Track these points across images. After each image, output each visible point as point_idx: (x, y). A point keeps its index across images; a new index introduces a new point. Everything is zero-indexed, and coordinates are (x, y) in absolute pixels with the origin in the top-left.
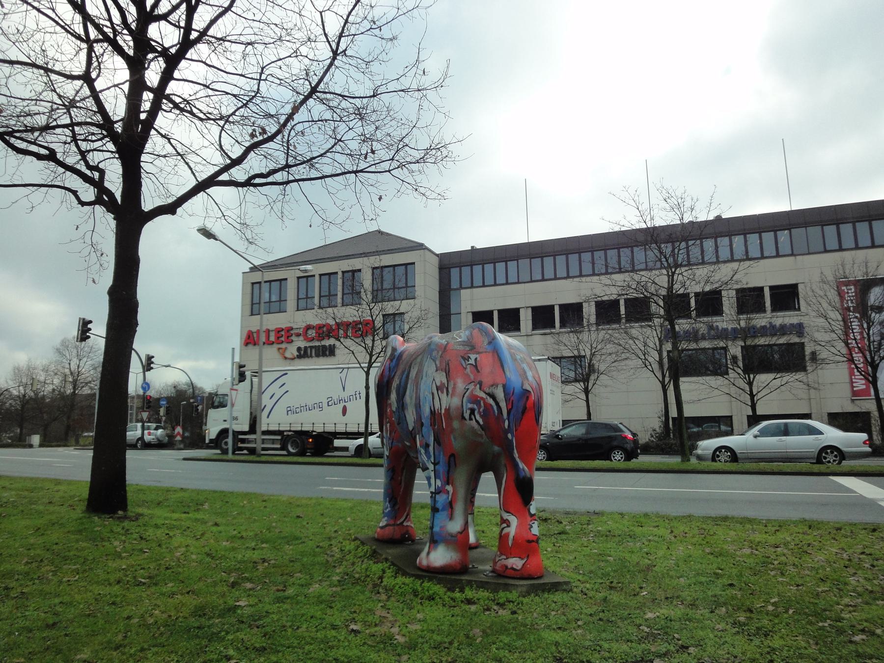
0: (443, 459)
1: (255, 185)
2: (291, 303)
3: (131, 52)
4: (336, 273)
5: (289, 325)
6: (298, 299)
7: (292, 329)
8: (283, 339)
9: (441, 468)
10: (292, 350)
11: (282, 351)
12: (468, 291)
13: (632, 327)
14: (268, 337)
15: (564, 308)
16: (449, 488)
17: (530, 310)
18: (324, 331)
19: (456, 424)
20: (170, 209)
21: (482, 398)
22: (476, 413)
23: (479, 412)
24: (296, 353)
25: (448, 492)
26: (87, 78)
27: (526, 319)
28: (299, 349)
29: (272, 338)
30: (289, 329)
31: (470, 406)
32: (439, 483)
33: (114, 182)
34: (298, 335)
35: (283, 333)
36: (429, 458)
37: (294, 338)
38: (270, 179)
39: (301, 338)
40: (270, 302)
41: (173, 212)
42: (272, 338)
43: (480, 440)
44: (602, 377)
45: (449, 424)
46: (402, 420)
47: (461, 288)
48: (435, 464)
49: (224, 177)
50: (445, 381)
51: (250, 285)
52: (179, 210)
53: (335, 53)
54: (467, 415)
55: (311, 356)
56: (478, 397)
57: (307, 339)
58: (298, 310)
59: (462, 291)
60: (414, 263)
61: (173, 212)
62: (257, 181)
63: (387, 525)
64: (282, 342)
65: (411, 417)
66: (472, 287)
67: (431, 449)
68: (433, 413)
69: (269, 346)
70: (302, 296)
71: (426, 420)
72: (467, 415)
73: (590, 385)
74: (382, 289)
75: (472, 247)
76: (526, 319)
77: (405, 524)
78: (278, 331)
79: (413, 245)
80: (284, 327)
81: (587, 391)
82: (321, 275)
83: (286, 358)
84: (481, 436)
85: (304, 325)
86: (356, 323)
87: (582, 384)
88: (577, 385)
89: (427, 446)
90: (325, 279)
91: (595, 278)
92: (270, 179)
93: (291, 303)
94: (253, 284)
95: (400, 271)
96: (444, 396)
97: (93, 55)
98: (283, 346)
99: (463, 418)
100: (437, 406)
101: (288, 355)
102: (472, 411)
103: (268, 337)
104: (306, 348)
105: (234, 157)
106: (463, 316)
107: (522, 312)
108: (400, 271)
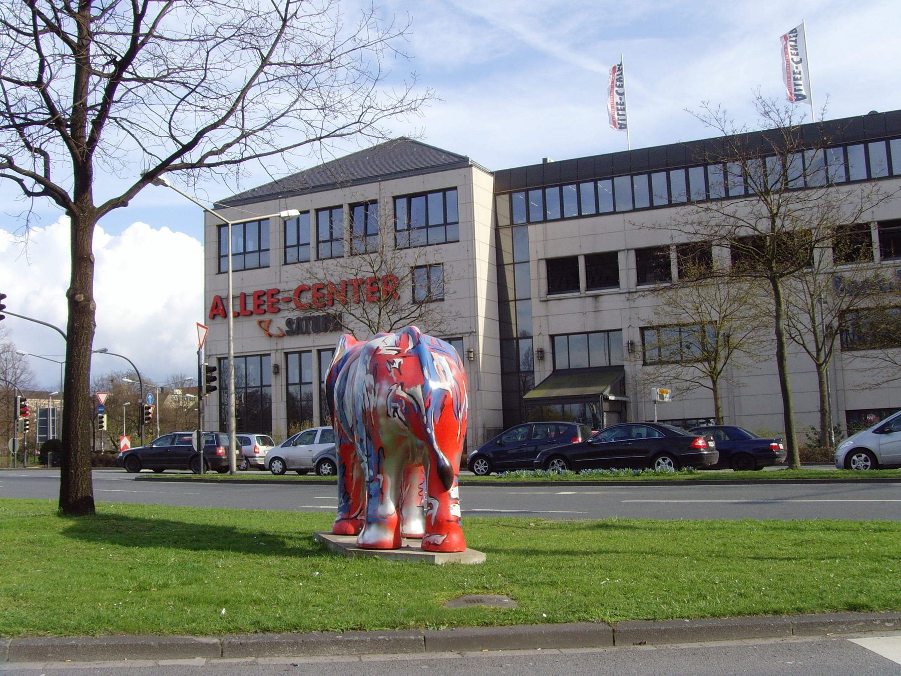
0: (373, 452)
1: (209, 166)
2: (275, 256)
3: (76, 40)
4: (341, 206)
5: (273, 287)
6: (286, 247)
7: (279, 292)
8: (265, 307)
9: (373, 460)
10: (279, 323)
11: (264, 326)
12: (540, 227)
13: (442, 352)
14: (244, 304)
15: (684, 249)
16: (380, 477)
17: (633, 254)
18: (323, 293)
19: (382, 421)
20: (121, 202)
21: (403, 398)
22: (399, 410)
23: (401, 410)
24: (285, 328)
25: (379, 480)
26: (39, 84)
27: (627, 267)
28: (289, 322)
29: (250, 307)
30: (274, 293)
31: (394, 404)
32: (372, 473)
33: (64, 176)
34: (288, 301)
35: (265, 298)
36: (363, 451)
37: (282, 306)
38: (224, 157)
39: (292, 305)
40: (245, 253)
41: (125, 204)
42: (250, 307)
43: (404, 434)
44: (736, 353)
45: (377, 422)
46: (343, 418)
47: (529, 222)
48: (368, 456)
49: (177, 161)
50: (373, 383)
51: (215, 229)
52: (130, 202)
53: (285, 20)
54: (391, 413)
55: (309, 333)
56: (399, 396)
57: (300, 307)
58: (286, 263)
59: (531, 228)
60: (455, 188)
61: (125, 204)
62: (208, 161)
63: (342, 519)
64: (265, 312)
65: (349, 418)
66: (545, 220)
67: (364, 443)
68: (364, 411)
69: (247, 318)
70: (292, 240)
71: (360, 419)
72: (391, 413)
73: (719, 366)
74: (427, 226)
75: (545, 160)
76: (627, 267)
77: (359, 518)
78: (259, 295)
79: (453, 160)
80: (264, 288)
81: (714, 375)
82: (317, 211)
83: (270, 336)
84: (404, 430)
85: (294, 286)
86: (374, 281)
87: (706, 364)
88: (700, 365)
89: (362, 440)
90: (325, 216)
91: (713, 206)
92: (224, 157)
93: (275, 256)
94: (395, 198)
95: (435, 201)
96: (372, 396)
97: (46, 64)
98: (266, 317)
99: (388, 415)
100: (367, 405)
101: (273, 330)
102: (396, 409)
103: (244, 304)
104: (299, 320)
105: (185, 143)
106: (533, 266)
107: (621, 257)
108: (435, 201)
